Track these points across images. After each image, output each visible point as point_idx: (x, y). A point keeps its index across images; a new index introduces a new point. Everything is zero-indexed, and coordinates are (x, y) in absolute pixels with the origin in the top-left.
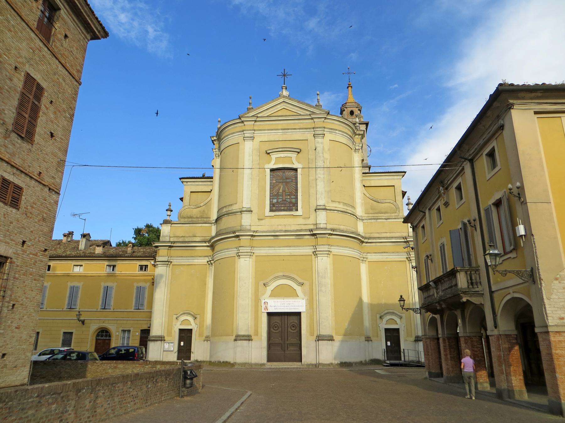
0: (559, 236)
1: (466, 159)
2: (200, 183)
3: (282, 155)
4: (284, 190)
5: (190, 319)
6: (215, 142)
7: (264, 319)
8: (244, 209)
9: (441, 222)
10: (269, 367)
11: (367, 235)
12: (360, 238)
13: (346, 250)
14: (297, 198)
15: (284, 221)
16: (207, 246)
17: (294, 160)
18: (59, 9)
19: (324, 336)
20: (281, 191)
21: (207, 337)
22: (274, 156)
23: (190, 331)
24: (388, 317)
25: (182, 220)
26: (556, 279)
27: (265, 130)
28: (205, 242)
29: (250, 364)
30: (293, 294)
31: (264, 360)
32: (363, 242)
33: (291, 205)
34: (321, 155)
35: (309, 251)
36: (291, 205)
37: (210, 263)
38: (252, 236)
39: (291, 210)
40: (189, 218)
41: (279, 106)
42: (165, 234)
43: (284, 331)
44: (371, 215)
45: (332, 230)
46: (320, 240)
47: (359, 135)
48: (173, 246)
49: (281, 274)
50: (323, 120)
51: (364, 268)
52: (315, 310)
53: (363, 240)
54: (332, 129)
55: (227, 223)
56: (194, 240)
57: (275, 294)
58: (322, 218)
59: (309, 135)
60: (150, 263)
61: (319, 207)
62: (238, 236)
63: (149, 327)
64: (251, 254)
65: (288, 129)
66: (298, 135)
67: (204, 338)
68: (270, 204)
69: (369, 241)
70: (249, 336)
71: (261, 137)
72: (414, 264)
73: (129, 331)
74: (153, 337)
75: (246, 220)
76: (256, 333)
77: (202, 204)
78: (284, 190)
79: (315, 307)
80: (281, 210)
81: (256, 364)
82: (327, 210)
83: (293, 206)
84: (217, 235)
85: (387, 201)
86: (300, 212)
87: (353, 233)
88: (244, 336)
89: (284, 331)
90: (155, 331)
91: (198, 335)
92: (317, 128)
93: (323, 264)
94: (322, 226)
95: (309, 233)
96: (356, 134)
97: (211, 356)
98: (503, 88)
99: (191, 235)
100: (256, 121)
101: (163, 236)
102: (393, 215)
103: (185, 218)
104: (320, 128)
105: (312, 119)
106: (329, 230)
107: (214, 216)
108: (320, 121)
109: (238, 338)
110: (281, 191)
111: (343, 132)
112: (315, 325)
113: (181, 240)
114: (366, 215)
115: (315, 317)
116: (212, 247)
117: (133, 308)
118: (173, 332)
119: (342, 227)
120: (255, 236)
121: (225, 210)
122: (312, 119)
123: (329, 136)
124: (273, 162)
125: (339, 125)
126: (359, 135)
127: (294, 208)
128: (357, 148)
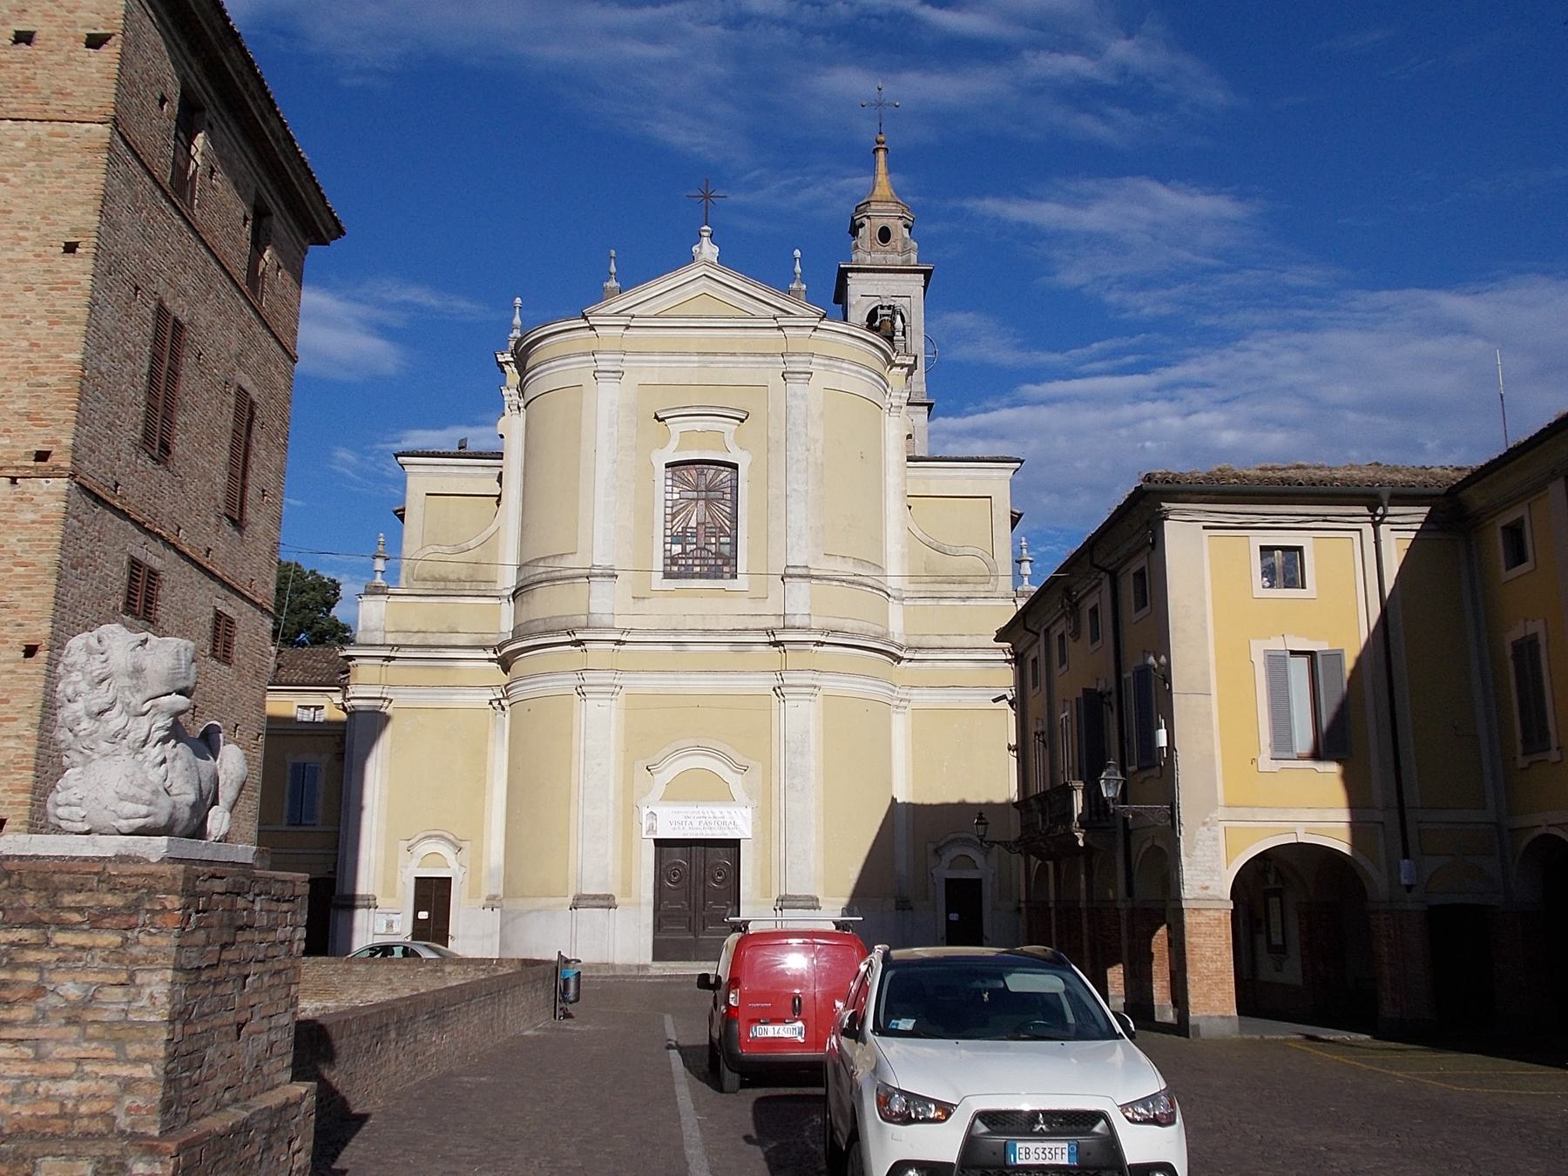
0: (1218, 752)
1: (1103, 569)
5: (446, 850)
6: (507, 368)
7: (648, 854)
9: (1065, 667)
10: (658, 973)
11: (914, 642)
12: (893, 650)
13: (853, 681)
14: (734, 544)
15: (700, 602)
16: (490, 660)
18: (271, 214)
19: (796, 898)
20: (693, 523)
21: (492, 898)
22: (677, 427)
23: (446, 882)
24: (956, 851)
25: (419, 584)
26: (1204, 824)
27: (652, 353)
28: (484, 648)
29: (613, 966)
31: (646, 956)
32: (899, 659)
33: (720, 562)
35: (764, 683)
36: (720, 562)
37: (498, 704)
38: (619, 642)
39: (718, 575)
40: (436, 580)
41: (690, 287)
42: (371, 625)
43: (696, 881)
44: (923, 587)
45: (822, 631)
46: (793, 659)
47: (902, 366)
48: (394, 658)
49: (693, 742)
50: (810, 331)
51: (900, 726)
52: (775, 834)
53: (900, 654)
54: (831, 358)
55: (546, 603)
56: (453, 642)
57: (674, 794)
58: (800, 600)
59: (770, 374)
61: (791, 571)
62: (579, 643)
63: (334, 872)
64: (613, 690)
65: (715, 354)
66: (742, 371)
67: (483, 901)
69: (917, 656)
70: (609, 897)
71: (643, 371)
72: (1013, 742)
75: (604, 601)
76: (627, 892)
77: (472, 544)
79: (775, 824)
80: (693, 576)
81: (629, 967)
82: (812, 577)
83: (722, 565)
84: (518, 634)
85: (969, 550)
86: (742, 582)
87: (876, 638)
88: (595, 897)
89: (696, 881)
92: (793, 354)
93: (801, 717)
94: (798, 622)
95: (766, 639)
96: (893, 365)
97: (503, 944)
98: (1152, 486)
99: (444, 628)
100: (628, 327)
101: (365, 630)
102: (980, 587)
103: (424, 580)
104: (800, 354)
105: (780, 328)
106: (816, 631)
107: (508, 580)
108: (802, 336)
109: (580, 902)
111: (863, 366)
112: (775, 871)
113: (415, 640)
114: (912, 587)
115: (775, 850)
116: (505, 664)
117: (285, 821)
118: (399, 885)
119: (849, 625)
120: (624, 642)
122: (780, 328)
123: (823, 377)
124: (674, 444)
125: (850, 345)
126: (902, 366)
127: (726, 569)
128: (896, 402)
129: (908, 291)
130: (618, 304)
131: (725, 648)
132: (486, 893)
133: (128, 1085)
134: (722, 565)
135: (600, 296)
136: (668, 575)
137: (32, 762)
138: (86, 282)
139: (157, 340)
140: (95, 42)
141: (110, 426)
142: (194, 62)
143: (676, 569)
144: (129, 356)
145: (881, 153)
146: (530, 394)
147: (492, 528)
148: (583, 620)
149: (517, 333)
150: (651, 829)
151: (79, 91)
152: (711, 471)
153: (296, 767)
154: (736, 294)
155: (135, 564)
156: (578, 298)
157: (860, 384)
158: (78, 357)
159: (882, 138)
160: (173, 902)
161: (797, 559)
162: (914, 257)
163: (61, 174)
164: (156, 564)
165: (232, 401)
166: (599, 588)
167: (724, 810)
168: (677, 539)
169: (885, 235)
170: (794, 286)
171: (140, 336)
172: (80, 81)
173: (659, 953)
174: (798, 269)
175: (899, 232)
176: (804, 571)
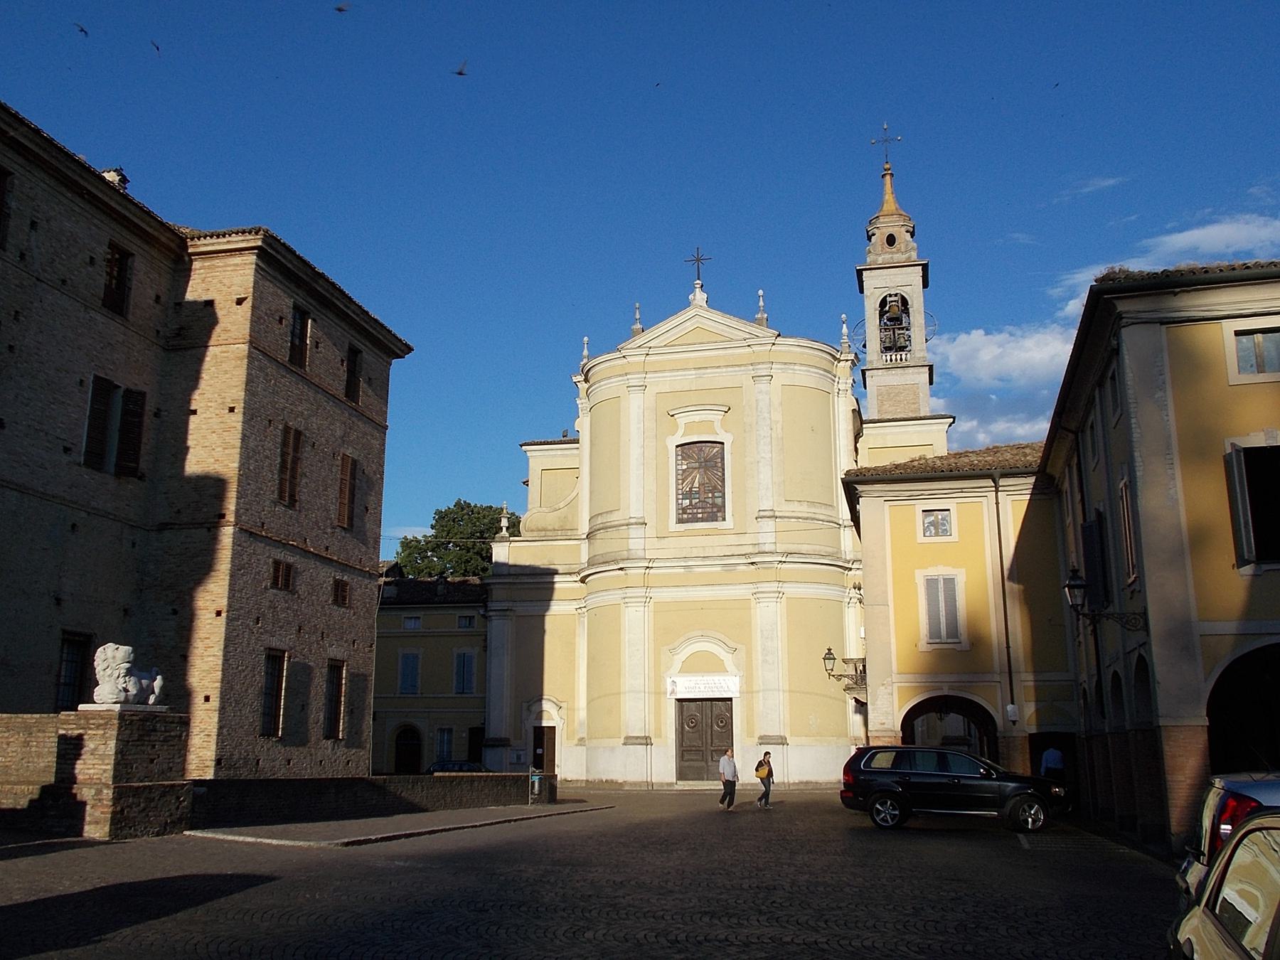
0: (893, 640)
2: (559, 452)
3: (697, 417)
4: (703, 483)
8: (633, 521)
15: (701, 537)
17: (717, 425)
20: (696, 484)
21: (582, 739)
22: (682, 420)
30: (719, 668)
34: (766, 415)
39: (715, 519)
41: (688, 324)
50: (769, 347)
55: (605, 545)
57: (687, 668)
58: (767, 534)
60: (476, 613)
61: (762, 514)
66: (724, 378)
67: (576, 741)
68: (678, 509)
70: (646, 738)
71: (662, 382)
73: (450, 731)
74: (492, 739)
75: (636, 541)
77: (561, 505)
78: (703, 483)
80: (698, 520)
83: (715, 512)
84: (591, 563)
86: (729, 523)
88: (637, 738)
90: (493, 731)
91: (565, 737)
97: (588, 771)
107: (584, 529)
109: (629, 741)
110: (696, 484)
119: (804, 548)
121: (600, 520)
124: (680, 432)
125: (802, 353)
129: (908, 282)
130: (640, 340)
131: (719, 569)
132: (577, 737)
133: (105, 771)
134: (715, 512)
135: (632, 335)
136: (680, 521)
137: (220, 668)
138: (239, 426)
139: (285, 444)
140: (240, 302)
141: (257, 495)
142: (300, 292)
143: (685, 516)
144: (267, 457)
145: (888, 177)
146: (594, 400)
147: (574, 494)
148: (625, 554)
149: (585, 361)
150: (673, 692)
151: (233, 328)
152: (706, 448)
153: (459, 655)
154: (718, 322)
155: (277, 563)
156: (612, 340)
157: (805, 377)
158: (236, 465)
159: (887, 166)
160: (116, 722)
161: (766, 505)
162: (914, 255)
163: (226, 372)
164: (291, 560)
165: (339, 463)
166: (635, 532)
167: (721, 678)
168: (688, 495)
169: (891, 240)
170: (759, 316)
171: (271, 446)
172: (233, 323)
173: (681, 775)
174: (761, 303)
175: (903, 237)
176: (771, 514)
